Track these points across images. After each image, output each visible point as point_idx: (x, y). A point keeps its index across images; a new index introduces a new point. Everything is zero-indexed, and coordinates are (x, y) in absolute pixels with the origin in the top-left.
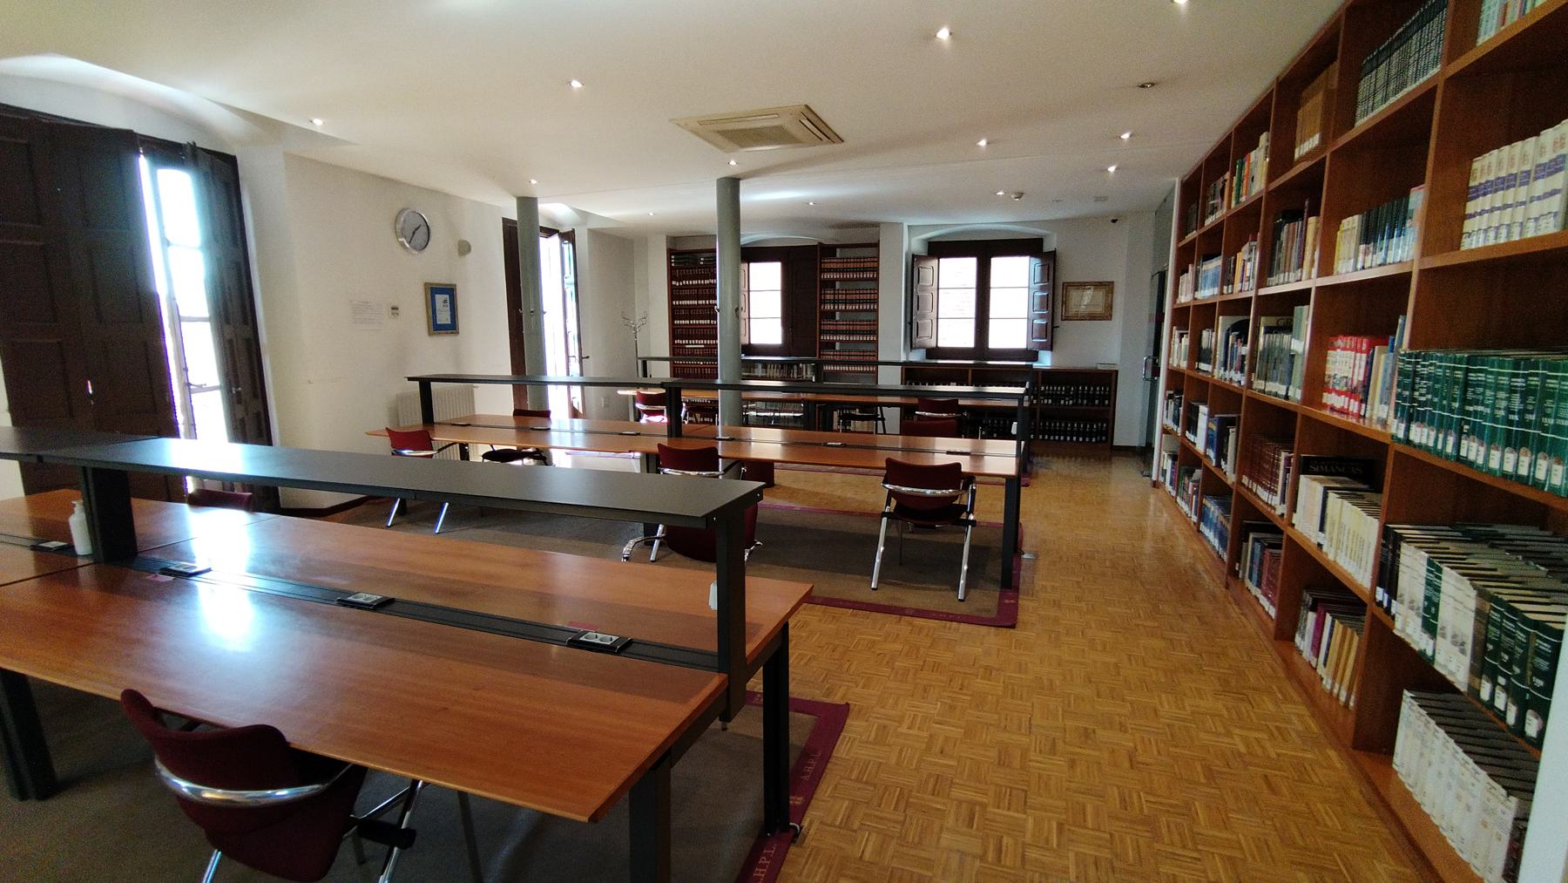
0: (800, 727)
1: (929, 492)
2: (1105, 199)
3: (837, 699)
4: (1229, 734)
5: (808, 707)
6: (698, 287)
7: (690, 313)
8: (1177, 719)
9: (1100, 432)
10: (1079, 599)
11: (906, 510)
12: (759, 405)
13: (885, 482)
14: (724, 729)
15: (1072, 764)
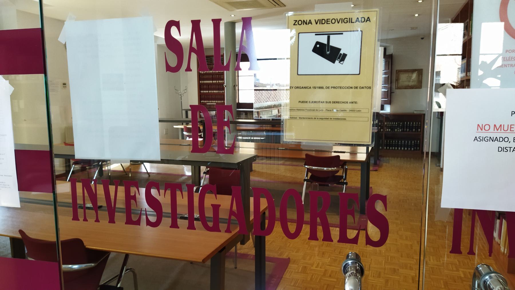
0: (269, 267)
1: (325, 169)
2: (417, 28)
3: (285, 256)
4: (458, 270)
5: (272, 260)
6: (212, 74)
7: (209, 87)
8: (437, 265)
9: (416, 145)
10: (397, 219)
11: (314, 178)
12: (244, 133)
13: (305, 165)
14: (236, 268)
15: (387, 281)
